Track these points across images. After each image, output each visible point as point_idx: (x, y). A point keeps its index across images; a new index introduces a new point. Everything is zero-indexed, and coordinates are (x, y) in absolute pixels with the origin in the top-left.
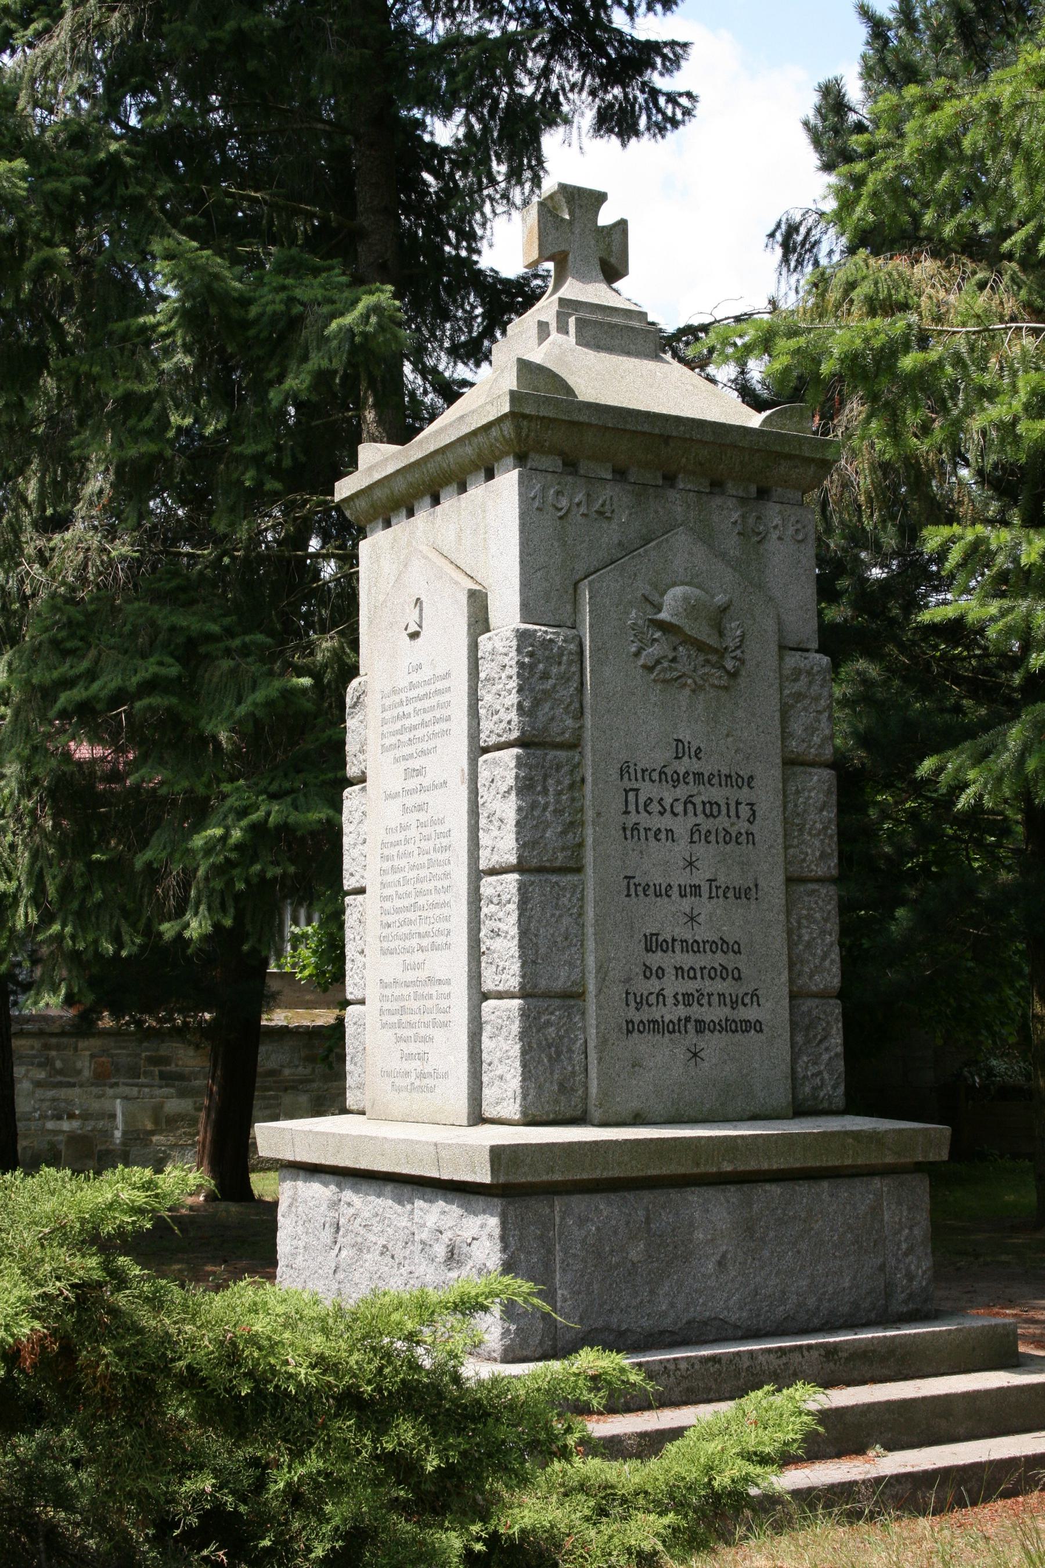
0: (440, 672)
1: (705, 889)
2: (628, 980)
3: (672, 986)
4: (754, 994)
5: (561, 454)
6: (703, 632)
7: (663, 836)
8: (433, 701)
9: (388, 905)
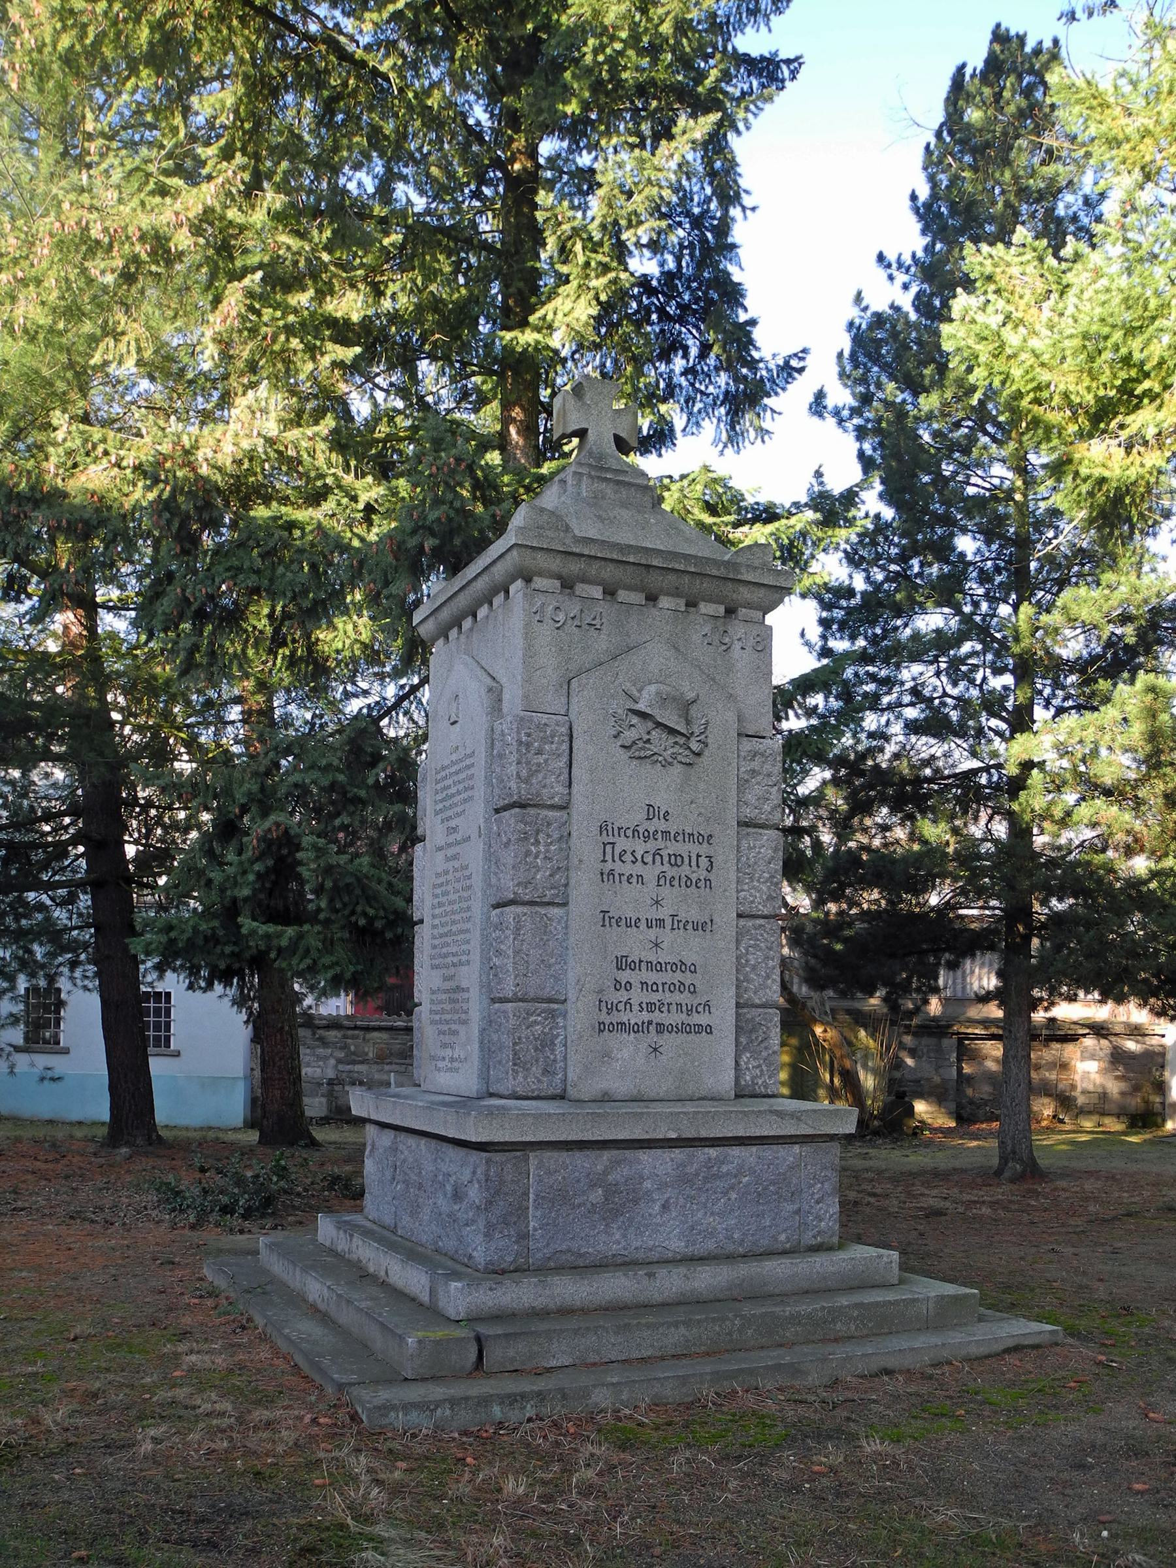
0: (468, 751)
1: (668, 922)
2: (601, 991)
3: (638, 996)
4: (707, 1005)
5: (559, 577)
6: (671, 719)
7: (634, 880)
8: (462, 776)
9: (436, 932)
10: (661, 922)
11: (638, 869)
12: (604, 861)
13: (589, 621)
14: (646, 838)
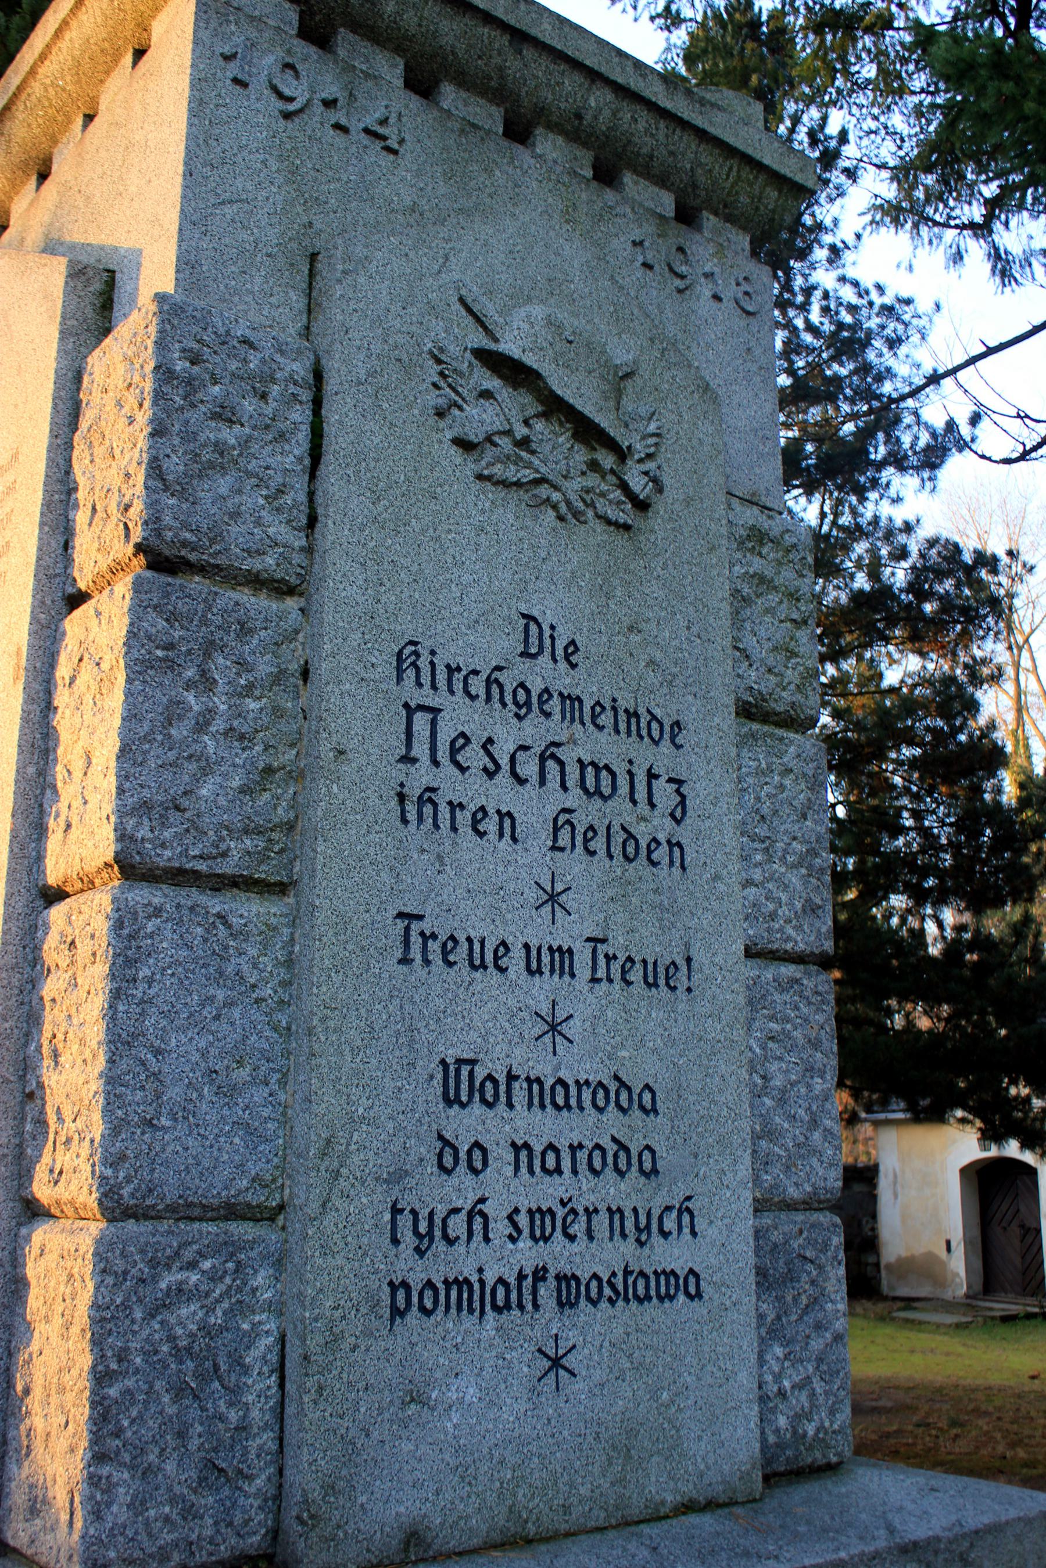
2: (398, 1176)
3: (506, 1189)
6: (583, 394)
7: (490, 825)
10: (562, 958)
11: (500, 793)
12: (408, 759)
13: (370, 121)
14: (522, 709)
